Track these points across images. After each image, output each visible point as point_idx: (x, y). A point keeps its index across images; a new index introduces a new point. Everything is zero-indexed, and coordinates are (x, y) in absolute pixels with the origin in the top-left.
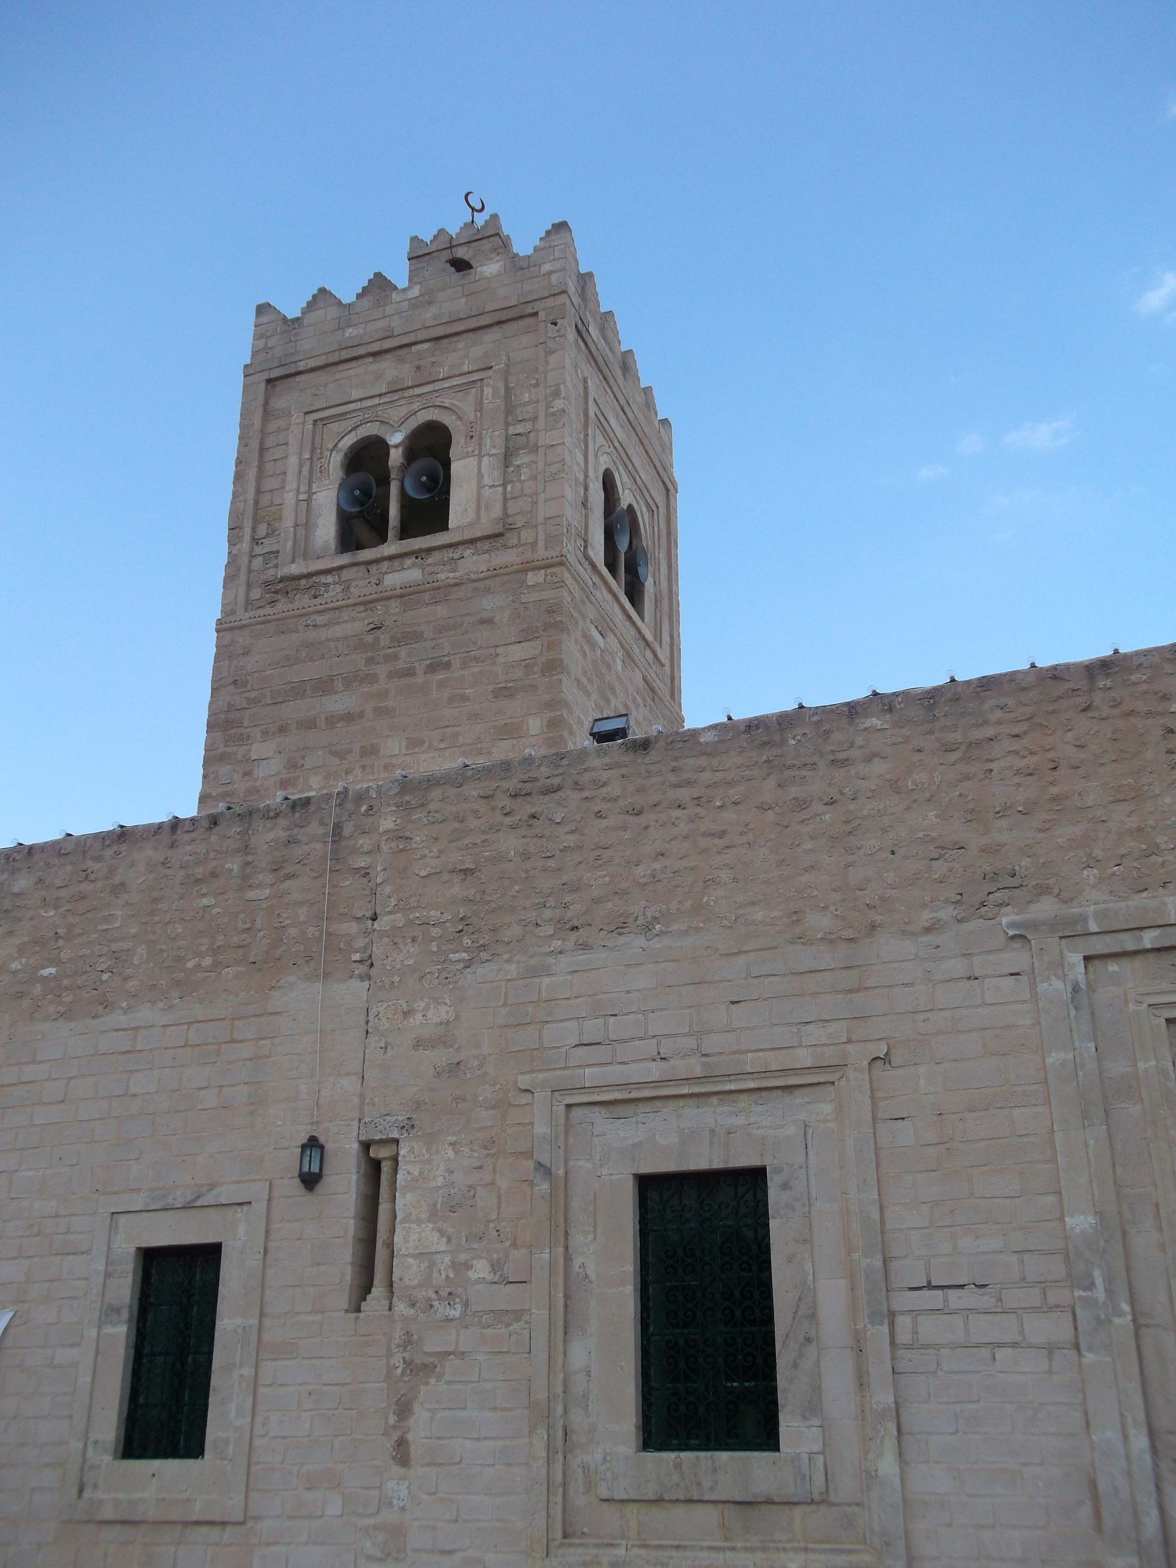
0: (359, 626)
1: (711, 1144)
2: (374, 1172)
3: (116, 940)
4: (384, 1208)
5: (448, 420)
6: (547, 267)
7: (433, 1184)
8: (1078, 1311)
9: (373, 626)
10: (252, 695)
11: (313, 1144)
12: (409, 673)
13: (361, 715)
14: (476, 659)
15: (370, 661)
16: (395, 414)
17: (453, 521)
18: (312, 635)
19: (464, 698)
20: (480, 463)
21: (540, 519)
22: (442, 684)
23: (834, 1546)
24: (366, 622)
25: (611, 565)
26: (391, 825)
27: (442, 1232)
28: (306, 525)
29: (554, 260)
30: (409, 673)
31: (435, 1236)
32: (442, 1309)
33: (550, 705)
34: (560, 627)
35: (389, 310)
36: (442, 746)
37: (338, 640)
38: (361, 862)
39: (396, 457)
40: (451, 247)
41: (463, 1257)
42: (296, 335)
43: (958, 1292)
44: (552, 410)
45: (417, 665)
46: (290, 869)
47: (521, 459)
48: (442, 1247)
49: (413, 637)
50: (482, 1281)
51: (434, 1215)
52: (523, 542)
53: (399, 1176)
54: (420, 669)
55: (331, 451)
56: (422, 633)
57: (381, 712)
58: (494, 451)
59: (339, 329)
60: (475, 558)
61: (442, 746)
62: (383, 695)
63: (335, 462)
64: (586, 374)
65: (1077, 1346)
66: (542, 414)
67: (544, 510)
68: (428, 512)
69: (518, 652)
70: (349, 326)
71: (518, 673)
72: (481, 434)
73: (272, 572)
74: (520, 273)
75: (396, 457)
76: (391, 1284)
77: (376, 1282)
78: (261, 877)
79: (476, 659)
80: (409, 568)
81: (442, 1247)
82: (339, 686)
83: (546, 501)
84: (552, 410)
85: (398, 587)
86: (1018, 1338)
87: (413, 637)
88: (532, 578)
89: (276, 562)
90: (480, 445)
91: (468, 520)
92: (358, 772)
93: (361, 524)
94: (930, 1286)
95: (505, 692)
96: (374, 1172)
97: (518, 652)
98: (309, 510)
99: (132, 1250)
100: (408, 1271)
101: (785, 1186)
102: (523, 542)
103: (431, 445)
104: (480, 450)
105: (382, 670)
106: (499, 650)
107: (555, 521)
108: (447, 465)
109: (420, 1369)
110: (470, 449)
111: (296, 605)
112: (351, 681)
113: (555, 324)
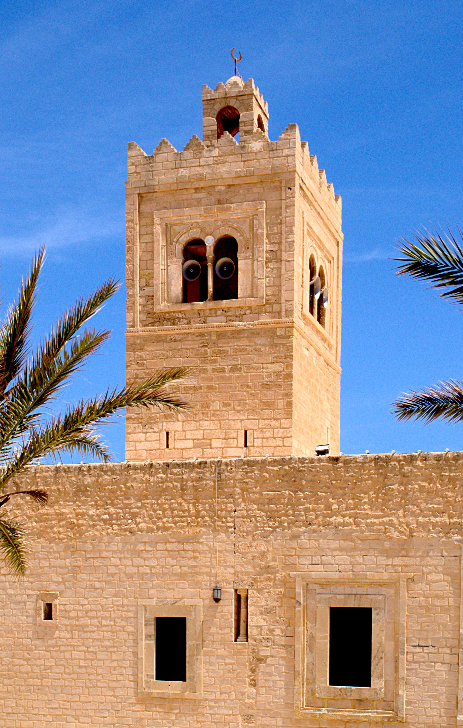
1: (355, 600)
2: (240, 601)
4: (243, 610)
5: (237, 236)
7: (260, 604)
8: (460, 655)
11: (216, 589)
14: (253, 368)
21: (283, 301)
23: (266, 327)
24: (200, 341)
25: (311, 312)
27: (264, 619)
29: (289, 148)
31: (262, 621)
32: (264, 643)
35: (202, 161)
36: (239, 408)
39: (210, 253)
40: (225, 98)
41: (272, 627)
43: (427, 648)
44: (288, 240)
48: (265, 624)
50: (277, 635)
51: (261, 613)
52: (274, 311)
53: (249, 601)
56: (228, 351)
57: (210, 388)
59: (176, 168)
60: (251, 315)
61: (239, 408)
64: (336, 364)
65: (458, 664)
66: (283, 241)
68: (227, 288)
70: (181, 168)
72: (253, 247)
74: (271, 152)
75: (210, 253)
76: (247, 634)
77: (241, 633)
79: (253, 368)
80: (219, 316)
81: (265, 624)
83: (286, 291)
84: (288, 240)
86: (442, 661)
89: (152, 301)
90: (253, 253)
91: (247, 294)
93: (193, 289)
94: (419, 646)
96: (240, 601)
99: (153, 617)
100: (252, 631)
101: (377, 614)
102: (274, 311)
103: (227, 246)
104: (253, 256)
106: (265, 366)
107: (290, 303)
108: (236, 260)
109: (260, 660)
110: (248, 255)
113: (290, 189)
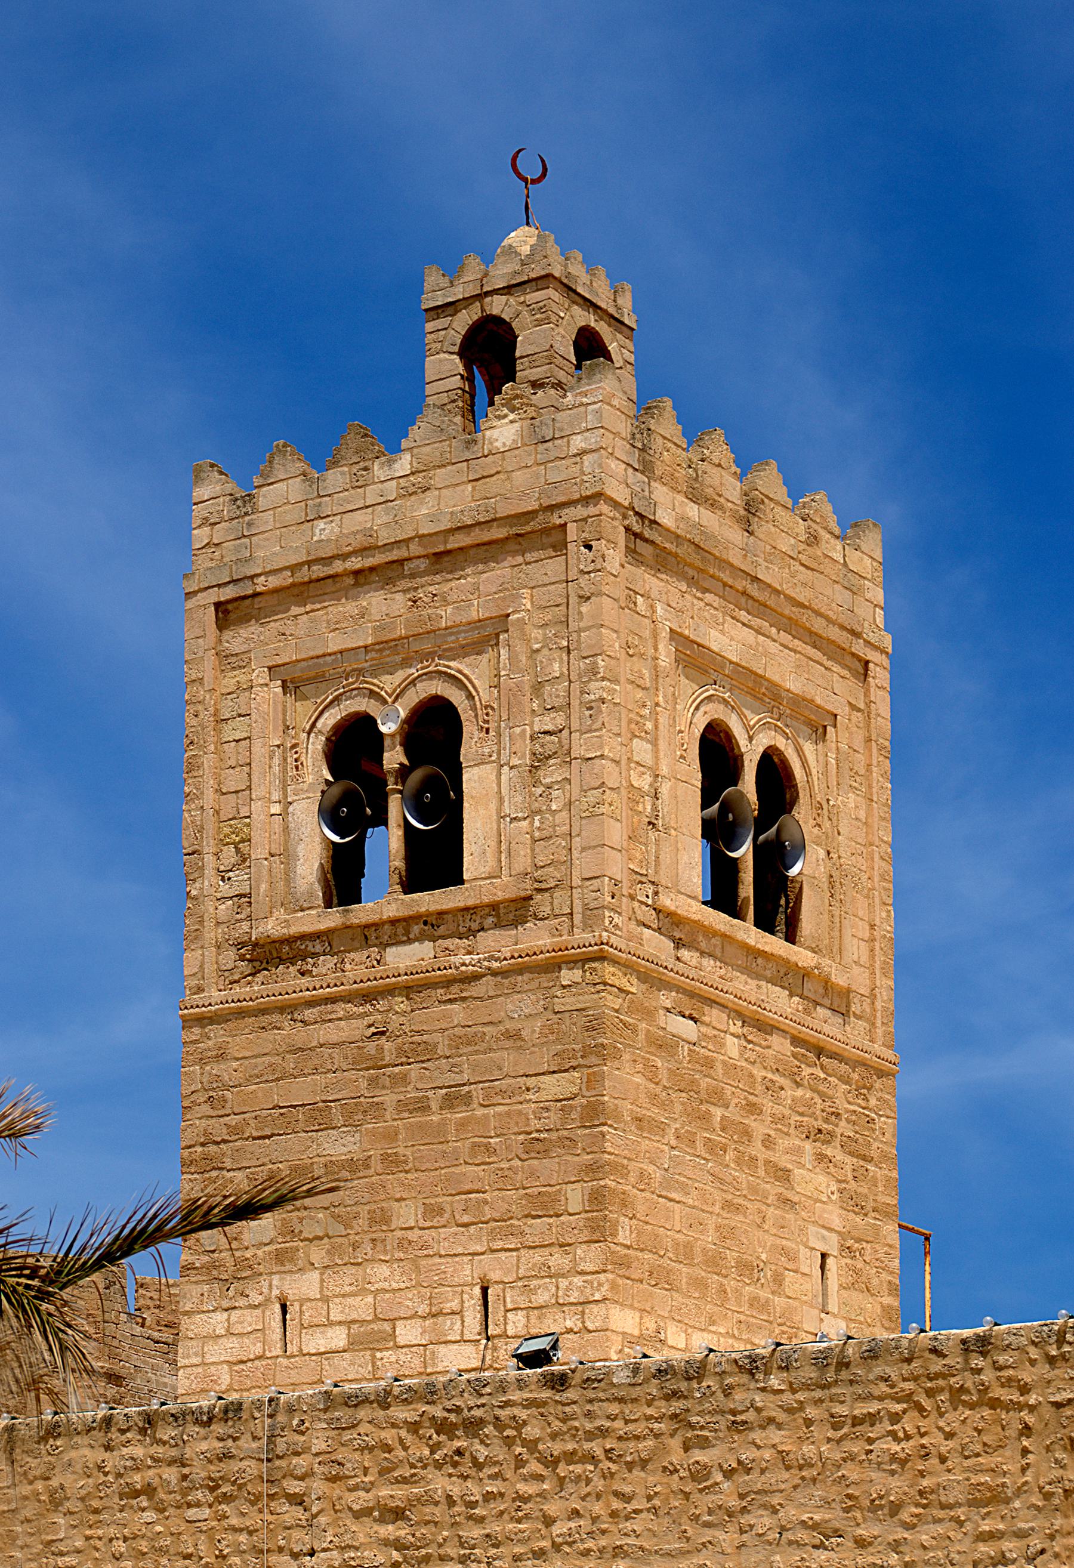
0: (355, 1029)
3: (62, 1554)
5: (456, 697)
6: (578, 442)
9: (373, 1030)
10: (233, 1120)
12: (421, 1106)
13: (366, 1163)
15: (373, 1082)
16: (388, 683)
17: (471, 866)
18: (300, 1035)
19: (489, 1149)
20: (499, 774)
22: (462, 1125)
26: (323, 1446)
28: (286, 855)
30: (421, 1106)
33: (593, 1170)
34: (602, 1052)
35: (371, 495)
37: (334, 1045)
38: (294, 1487)
42: (250, 524)
45: (430, 1093)
46: (226, 1489)
47: (552, 774)
49: (420, 1052)
54: (435, 1099)
55: (309, 734)
57: (393, 1163)
58: (515, 761)
61: (466, 1219)
62: (391, 1136)
63: (317, 745)
67: (583, 865)
69: (554, 1086)
71: (553, 1118)
73: (245, 926)
78: (199, 1495)
82: (337, 1115)
83: (583, 850)
85: (402, 972)
87: (420, 1052)
88: (567, 976)
92: (368, 1247)
95: (536, 1147)
97: (554, 1086)
98: (286, 829)
103: (436, 730)
105: (389, 1099)
108: (456, 772)
110: (487, 750)
111: (277, 987)
112: (357, 1112)
113: (589, 547)
